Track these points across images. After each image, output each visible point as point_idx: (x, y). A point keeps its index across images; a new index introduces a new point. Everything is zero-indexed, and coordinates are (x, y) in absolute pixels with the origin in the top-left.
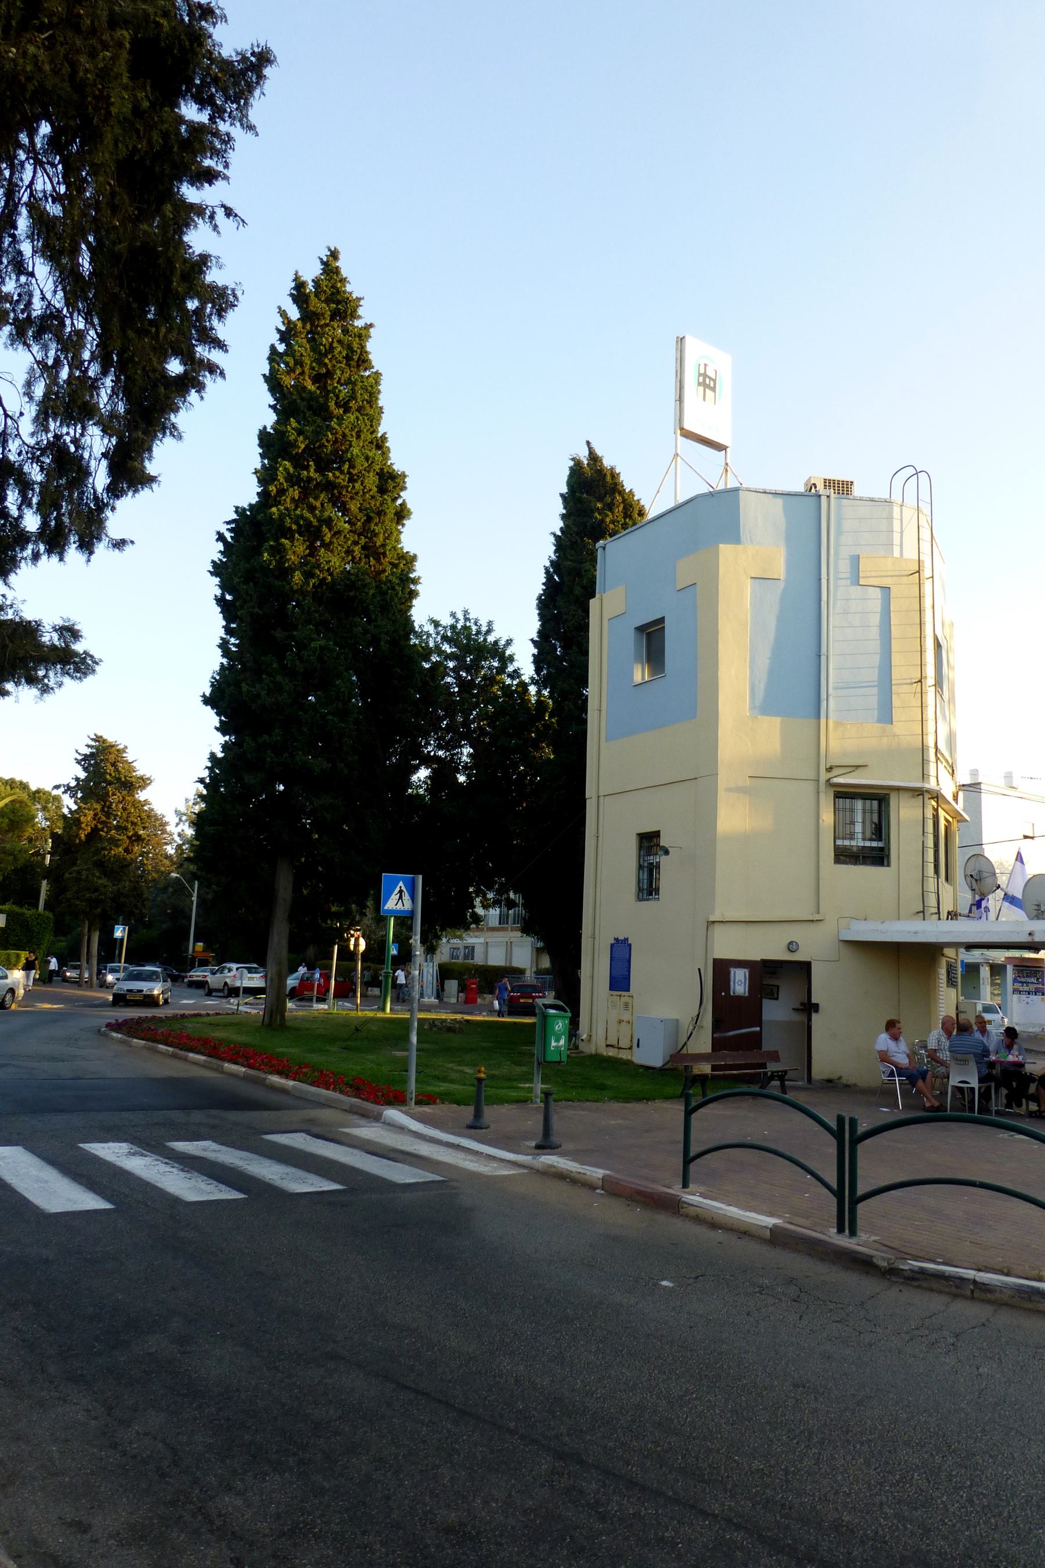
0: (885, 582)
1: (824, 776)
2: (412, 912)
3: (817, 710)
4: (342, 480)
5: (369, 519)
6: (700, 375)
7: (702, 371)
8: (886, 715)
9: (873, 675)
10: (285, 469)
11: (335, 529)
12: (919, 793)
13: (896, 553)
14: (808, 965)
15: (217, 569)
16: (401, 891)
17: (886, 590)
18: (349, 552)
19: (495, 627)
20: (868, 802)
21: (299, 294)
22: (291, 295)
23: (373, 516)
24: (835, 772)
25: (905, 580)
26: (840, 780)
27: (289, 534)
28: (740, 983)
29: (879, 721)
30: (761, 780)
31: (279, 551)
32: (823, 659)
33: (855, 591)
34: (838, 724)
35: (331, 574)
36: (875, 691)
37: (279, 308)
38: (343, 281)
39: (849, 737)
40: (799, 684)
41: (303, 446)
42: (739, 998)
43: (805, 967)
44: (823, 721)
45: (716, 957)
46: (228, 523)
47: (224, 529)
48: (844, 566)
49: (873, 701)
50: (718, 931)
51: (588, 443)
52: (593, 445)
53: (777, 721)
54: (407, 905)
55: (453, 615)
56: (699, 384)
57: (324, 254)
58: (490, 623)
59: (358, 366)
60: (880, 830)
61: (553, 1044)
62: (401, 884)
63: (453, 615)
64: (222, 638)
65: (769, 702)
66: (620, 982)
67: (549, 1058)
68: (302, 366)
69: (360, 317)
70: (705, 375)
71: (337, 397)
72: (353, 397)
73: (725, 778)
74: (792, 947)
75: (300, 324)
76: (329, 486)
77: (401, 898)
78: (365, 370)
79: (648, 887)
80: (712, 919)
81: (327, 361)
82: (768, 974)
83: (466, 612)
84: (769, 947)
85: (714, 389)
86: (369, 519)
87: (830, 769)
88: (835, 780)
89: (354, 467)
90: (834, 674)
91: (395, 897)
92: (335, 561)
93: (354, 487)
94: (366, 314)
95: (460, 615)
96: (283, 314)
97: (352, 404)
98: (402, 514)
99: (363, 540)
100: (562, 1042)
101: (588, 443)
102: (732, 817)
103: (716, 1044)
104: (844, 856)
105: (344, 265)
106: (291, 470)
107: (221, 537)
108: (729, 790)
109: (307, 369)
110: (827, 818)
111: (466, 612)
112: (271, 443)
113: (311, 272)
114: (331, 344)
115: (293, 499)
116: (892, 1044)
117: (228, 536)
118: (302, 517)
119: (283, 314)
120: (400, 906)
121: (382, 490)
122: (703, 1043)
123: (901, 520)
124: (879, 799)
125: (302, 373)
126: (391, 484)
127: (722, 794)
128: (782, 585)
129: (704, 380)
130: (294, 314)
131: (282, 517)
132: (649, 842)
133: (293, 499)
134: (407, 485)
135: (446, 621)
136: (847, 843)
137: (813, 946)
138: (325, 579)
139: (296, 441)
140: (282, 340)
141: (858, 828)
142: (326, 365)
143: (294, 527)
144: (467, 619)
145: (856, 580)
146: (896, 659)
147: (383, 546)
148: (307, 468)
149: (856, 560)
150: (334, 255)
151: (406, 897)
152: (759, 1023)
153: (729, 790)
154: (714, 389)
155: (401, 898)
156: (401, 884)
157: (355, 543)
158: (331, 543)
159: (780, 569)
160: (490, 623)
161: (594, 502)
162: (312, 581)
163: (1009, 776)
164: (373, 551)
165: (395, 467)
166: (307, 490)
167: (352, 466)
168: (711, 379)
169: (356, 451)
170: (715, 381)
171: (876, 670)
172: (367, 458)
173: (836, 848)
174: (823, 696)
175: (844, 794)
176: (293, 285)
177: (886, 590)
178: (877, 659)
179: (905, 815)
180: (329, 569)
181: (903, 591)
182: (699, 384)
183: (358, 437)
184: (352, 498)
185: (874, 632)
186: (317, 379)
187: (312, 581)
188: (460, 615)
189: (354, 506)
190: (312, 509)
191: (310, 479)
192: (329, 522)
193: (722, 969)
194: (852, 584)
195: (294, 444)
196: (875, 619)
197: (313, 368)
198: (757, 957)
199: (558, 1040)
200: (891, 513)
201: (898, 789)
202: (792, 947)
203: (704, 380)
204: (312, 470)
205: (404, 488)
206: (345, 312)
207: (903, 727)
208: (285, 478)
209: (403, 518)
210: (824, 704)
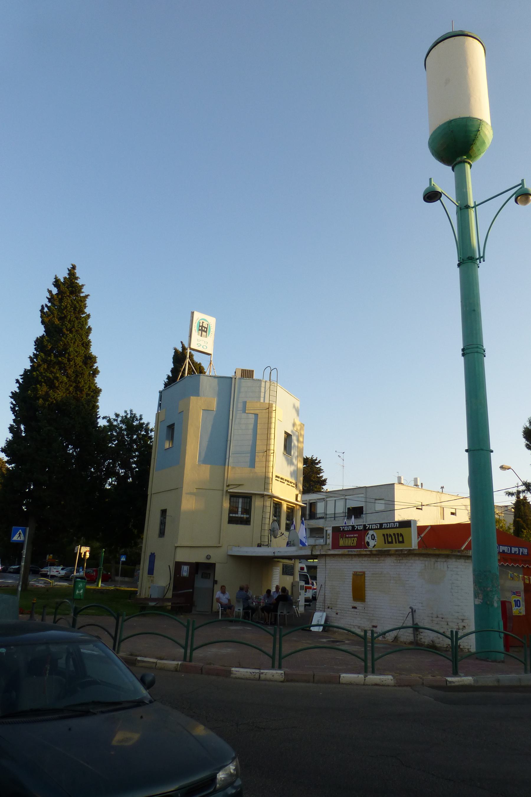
0: (256, 412)
1: (225, 488)
2: (24, 541)
3: (224, 462)
4: (65, 361)
5: (77, 376)
6: (200, 326)
7: (201, 325)
8: (252, 464)
9: (249, 449)
10: (41, 357)
11: (60, 381)
12: (263, 496)
13: (262, 400)
14: (215, 564)
15: (14, 395)
16: (20, 533)
17: (256, 415)
18: (67, 389)
19: (143, 417)
20: (246, 499)
21: (57, 283)
22: (53, 284)
23: (78, 374)
24: (229, 488)
25: (264, 411)
26: (231, 491)
27: (40, 383)
28: (185, 571)
29: (250, 467)
30: (201, 491)
31: (35, 390)
32: (229, 442)
33: (244, 415)
34: (233, 468)
35: (55, 400)
36: (249, 455)
37: (48, 289)
38: (77, 278)
39: (236, 472)
40: (218, 452)
41: (50, 347)
42: (184, 578)
43: (212, 566)
44: (226, 467)
45: (177, 560)
46: (21, 376)
47: (19, 378)
48: (240, 406)
49: (248, 459)
50: (178, 550)
51: (182, 342)
52: (184, 343)
53: (208, 467)
54: (22, 538)
55: (126, 412)
56: (199, 330)
57: (70, 267)
58: (141, 416)
59: (79, 313)
60: (247, 511)
61: (77, 592)
62: (20, 531)
63: (126, 412)
64: (11, 425)
65: (206, 459)
66: (151, 571)
67: (75, 597)
68: (53, 314)
69: (82, 292)
70: (202, 326)
71: (67, 327)
72: (73, 327)
73: (186, 488)
74: (208, 557)
75: (55, 297)
76: (59, 363)
77: (20, 536)
78: (83, 314)
79: (162, 533)
80: (176, 545)
81: (64, 312)
82: (196, 567)
83: (131, 411)
84: (199, 557)
85: (206, 332)
86: (77, 376)
87: (228, 486)
88: (229, 490)
89: (70, 356)
90: (233, 448)
91: (17, 535)
92: (59, 395)
93: (70, 364)
94: (85, 291)
95: (129, 412)
96: (50, 292)
97: (73, 329)
98: (96, 372)
99: (74, 385)
100: (81, 591)
101: (182, 342)
102: (188, 504)
103: (173, 595)
104: (232, 521)
105: (78, 272)
106: (44, 357)
107: (17, 381)
108: (187, 494)
109: (55, 315)
110: (226, 505)
111: (131, 411)
112: (39, 343)
113: (63, 275)
114: (66, 305)
115: (44, 369)
116: (221, 595)
117: (21, 381)
118: (46, 376)
119: (50, 292)
120: (19, 539)
121: (85, 363)
122: (169, 595)
123: (265, 387)
124: (248, 498)
125: (54, 317)
126: (89, 361)
127: (184, 495)
128: (215, 413)
129: (202, 328)
130: (55, 291)
131: (38, 376)
132: (164, 512)
133: (44, 369)
134: (97, 361)
135: (122, 414)
136: (234, 515)
137: (217, 557)
138: (53, 402)
139: (47, 345)
140: (49, 301)
141: (240, 510)
142: (64, 313)
143: (43, 380)
144: (131, 414)
145: (244, 411)
146: (258, 442)
147: (83, 386)
148: (50, 356)
149: (245, 403)
150: (74, 267)
151: (22, 535)
152: (193, 588)
153: (187, 494)
154: (206, 332)
155: (20, 536)
156: (20, 531)
157: (71, 386)
158: (59, 386)
159: (214, 406)
160: (141, 416)
161: (183, 367)
162: (47, 403)
163: (416, 480)
164: (78, 388)
165: (93, 354)
166: (50, 364)
167: (69, 355)
168: (205, 327)
169: (71, 349)
170: (207, 328)
171: (250, 447)
172: (77, 352)
173: (230, 518)
174: (227, 457)
175: (233, 496)
176: (54, 280)
177: (256, 415)
178: (251, 442)
179: (257, 503)
180: (54, 398)
181: (262, 416)
182: (199, 330)
183: (74, 343)
184: (70, 368)
185: (250, 432)
186: (60, 319)
187: (47, 403)
188: (129, 412)
189: (70, 371)
190: (52, 372)
191: (51, 361)
192: (57, 378)
193: (178, 565)
194: (243, 412)
195: (46, 346)
196: (251, 427)
197: (58, 315)
198: (194, 561)
199: (79, 591)
200: (261, 384)
201: (255, 494)
202: (208, 557)
203: (202, 328)
204: (52, 357)
205: (96, 362)
206: (76, 291)
207: (259, 469)
208: (41, 360)
209: (95, 374)
210: (227, 460)
